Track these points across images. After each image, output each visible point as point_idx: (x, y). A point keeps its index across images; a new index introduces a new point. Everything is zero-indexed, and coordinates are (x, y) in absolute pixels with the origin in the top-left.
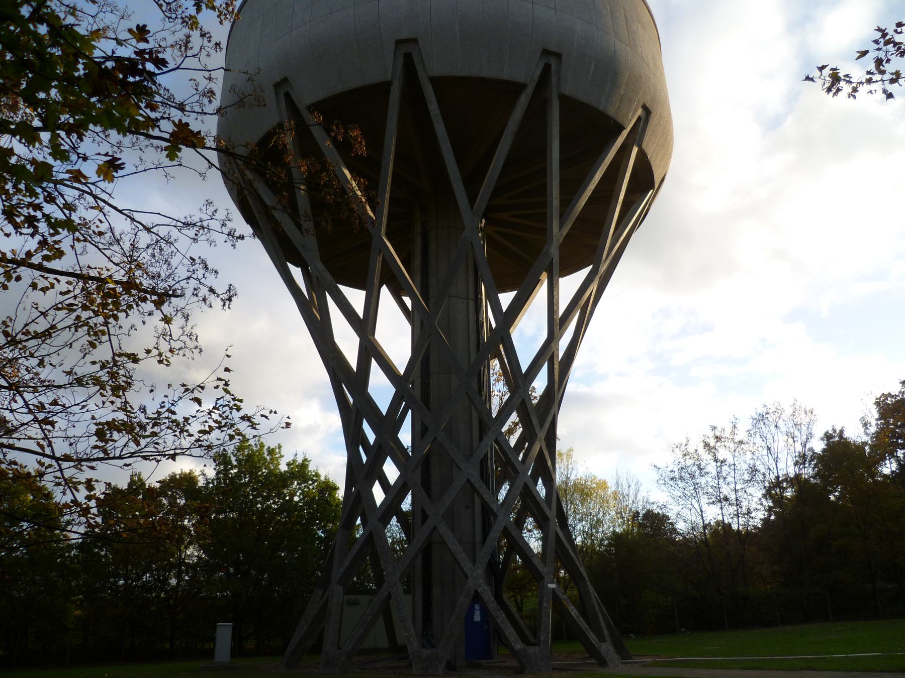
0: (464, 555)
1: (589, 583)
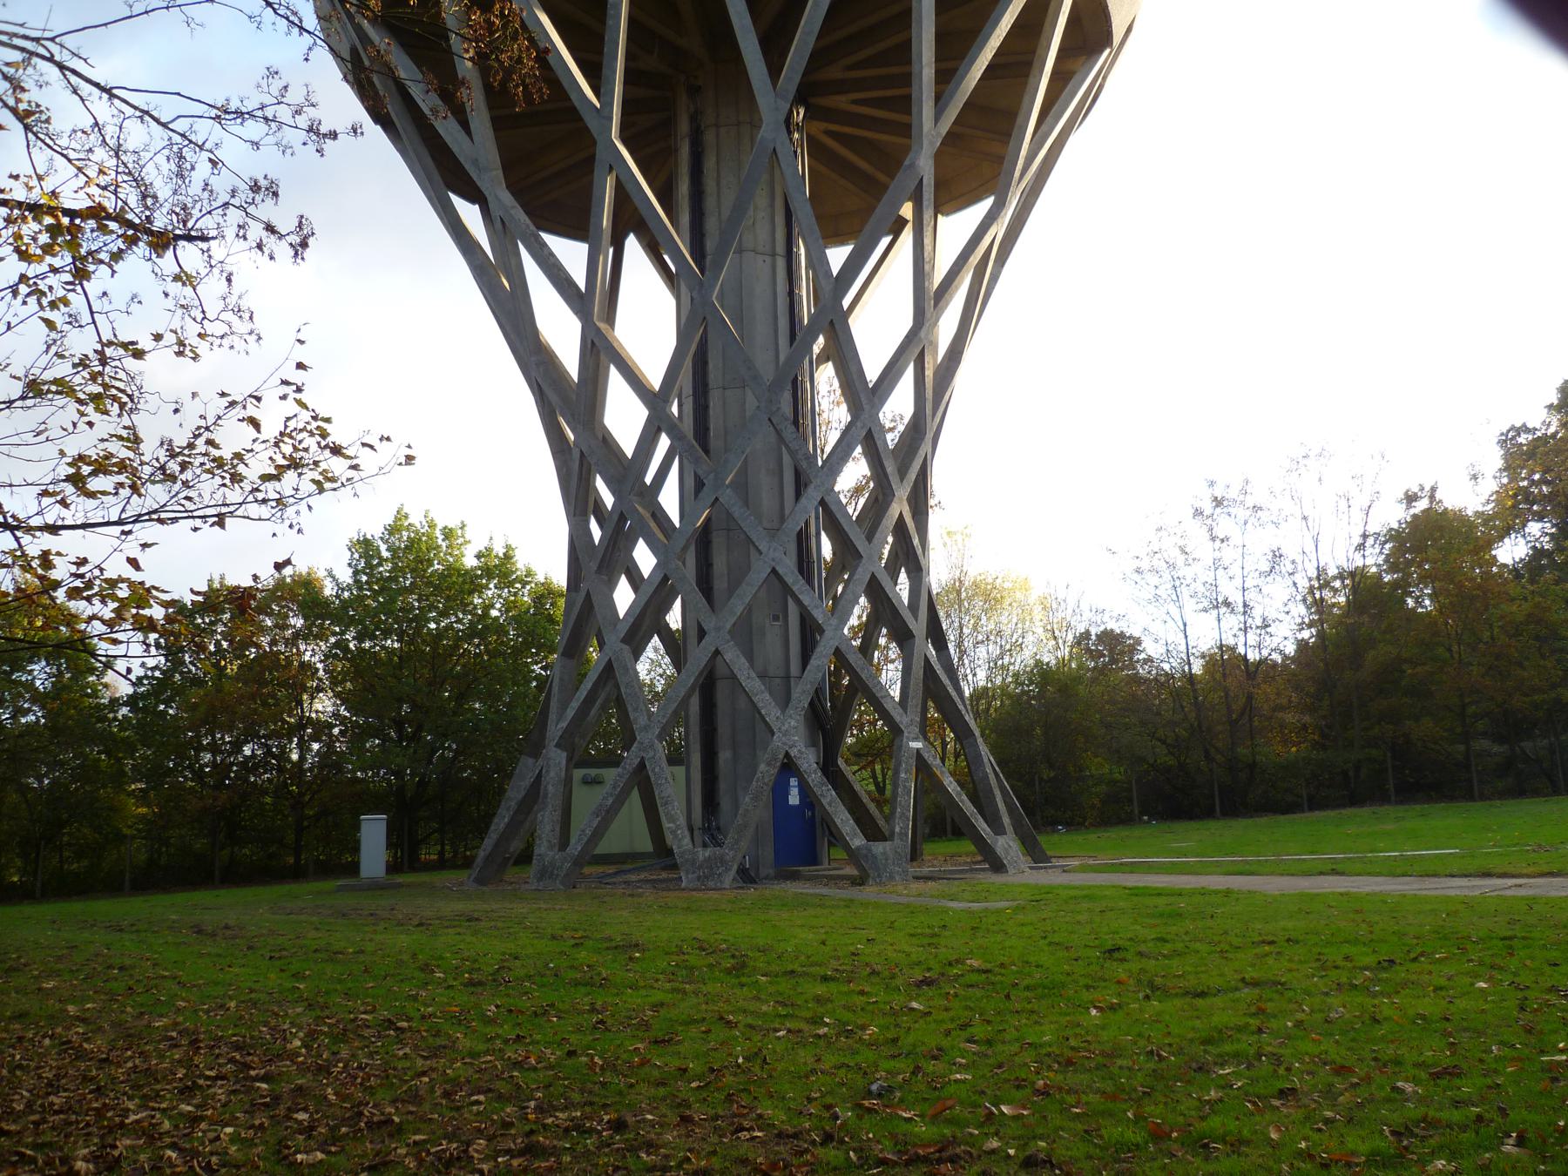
0: (767, 696)
1: (980, 740)
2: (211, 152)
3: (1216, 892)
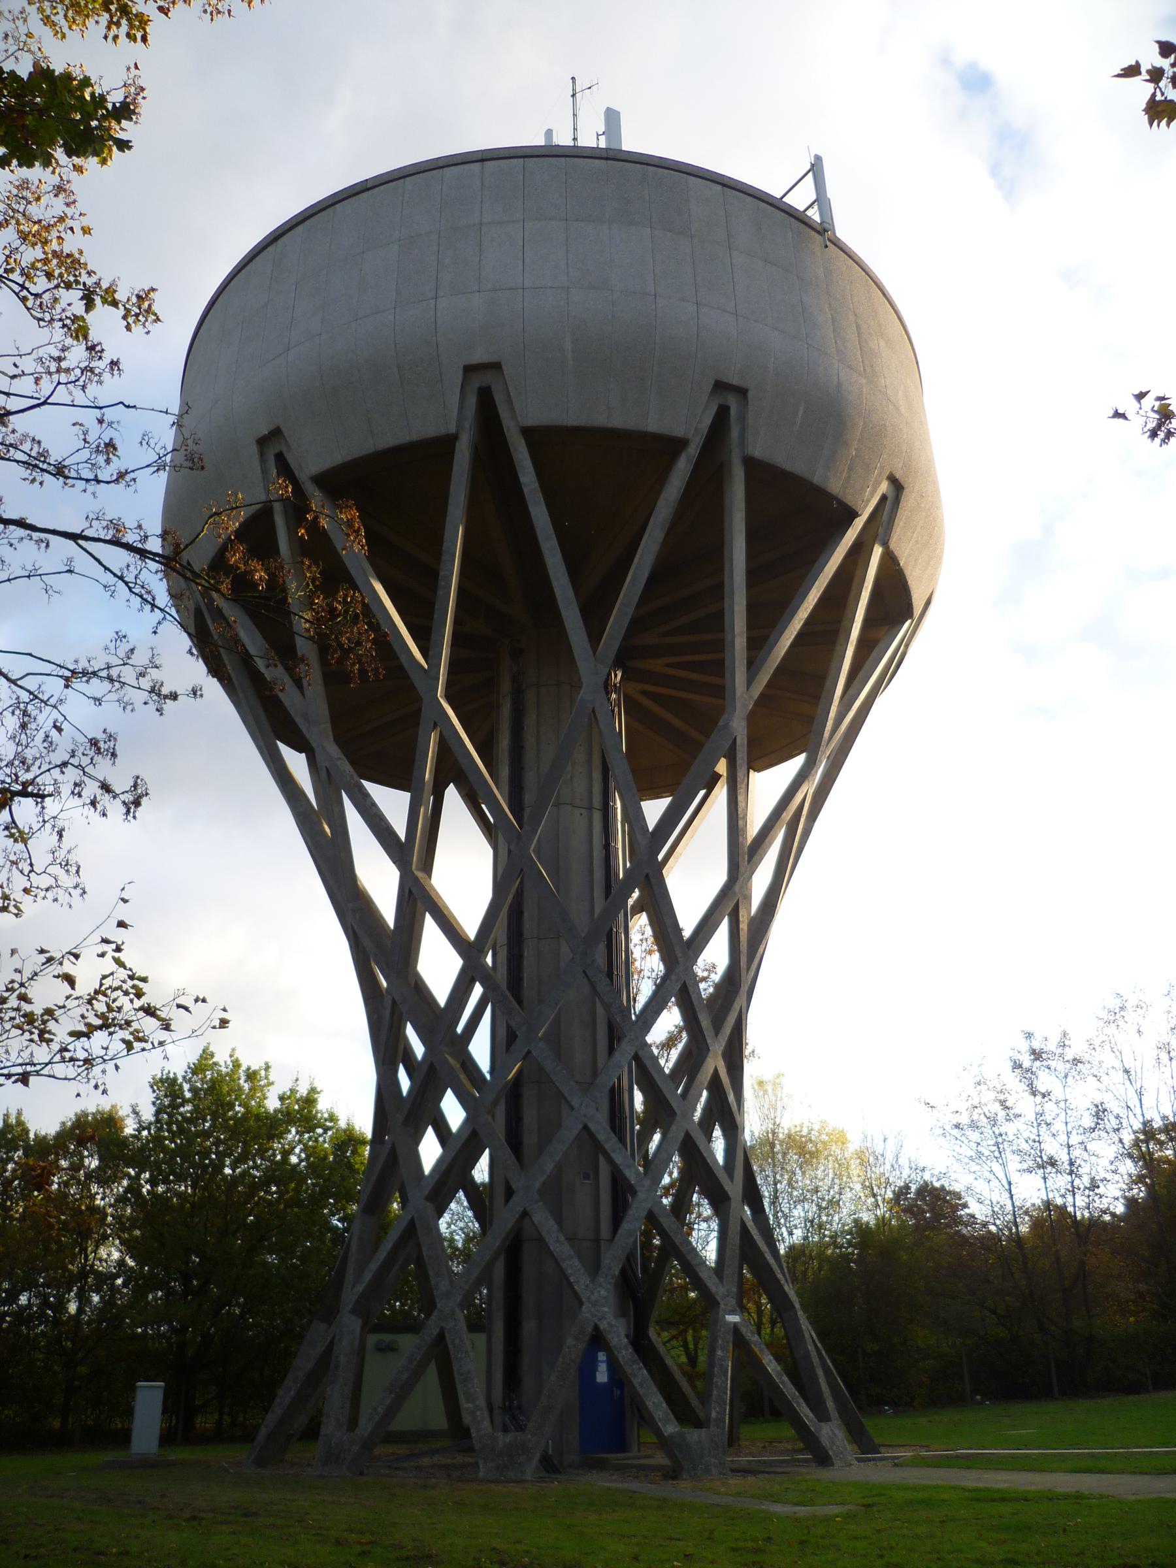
0: (576, 1262)
1: (800, 1313)
2: (55, 707)
3: (1066, 1497)
